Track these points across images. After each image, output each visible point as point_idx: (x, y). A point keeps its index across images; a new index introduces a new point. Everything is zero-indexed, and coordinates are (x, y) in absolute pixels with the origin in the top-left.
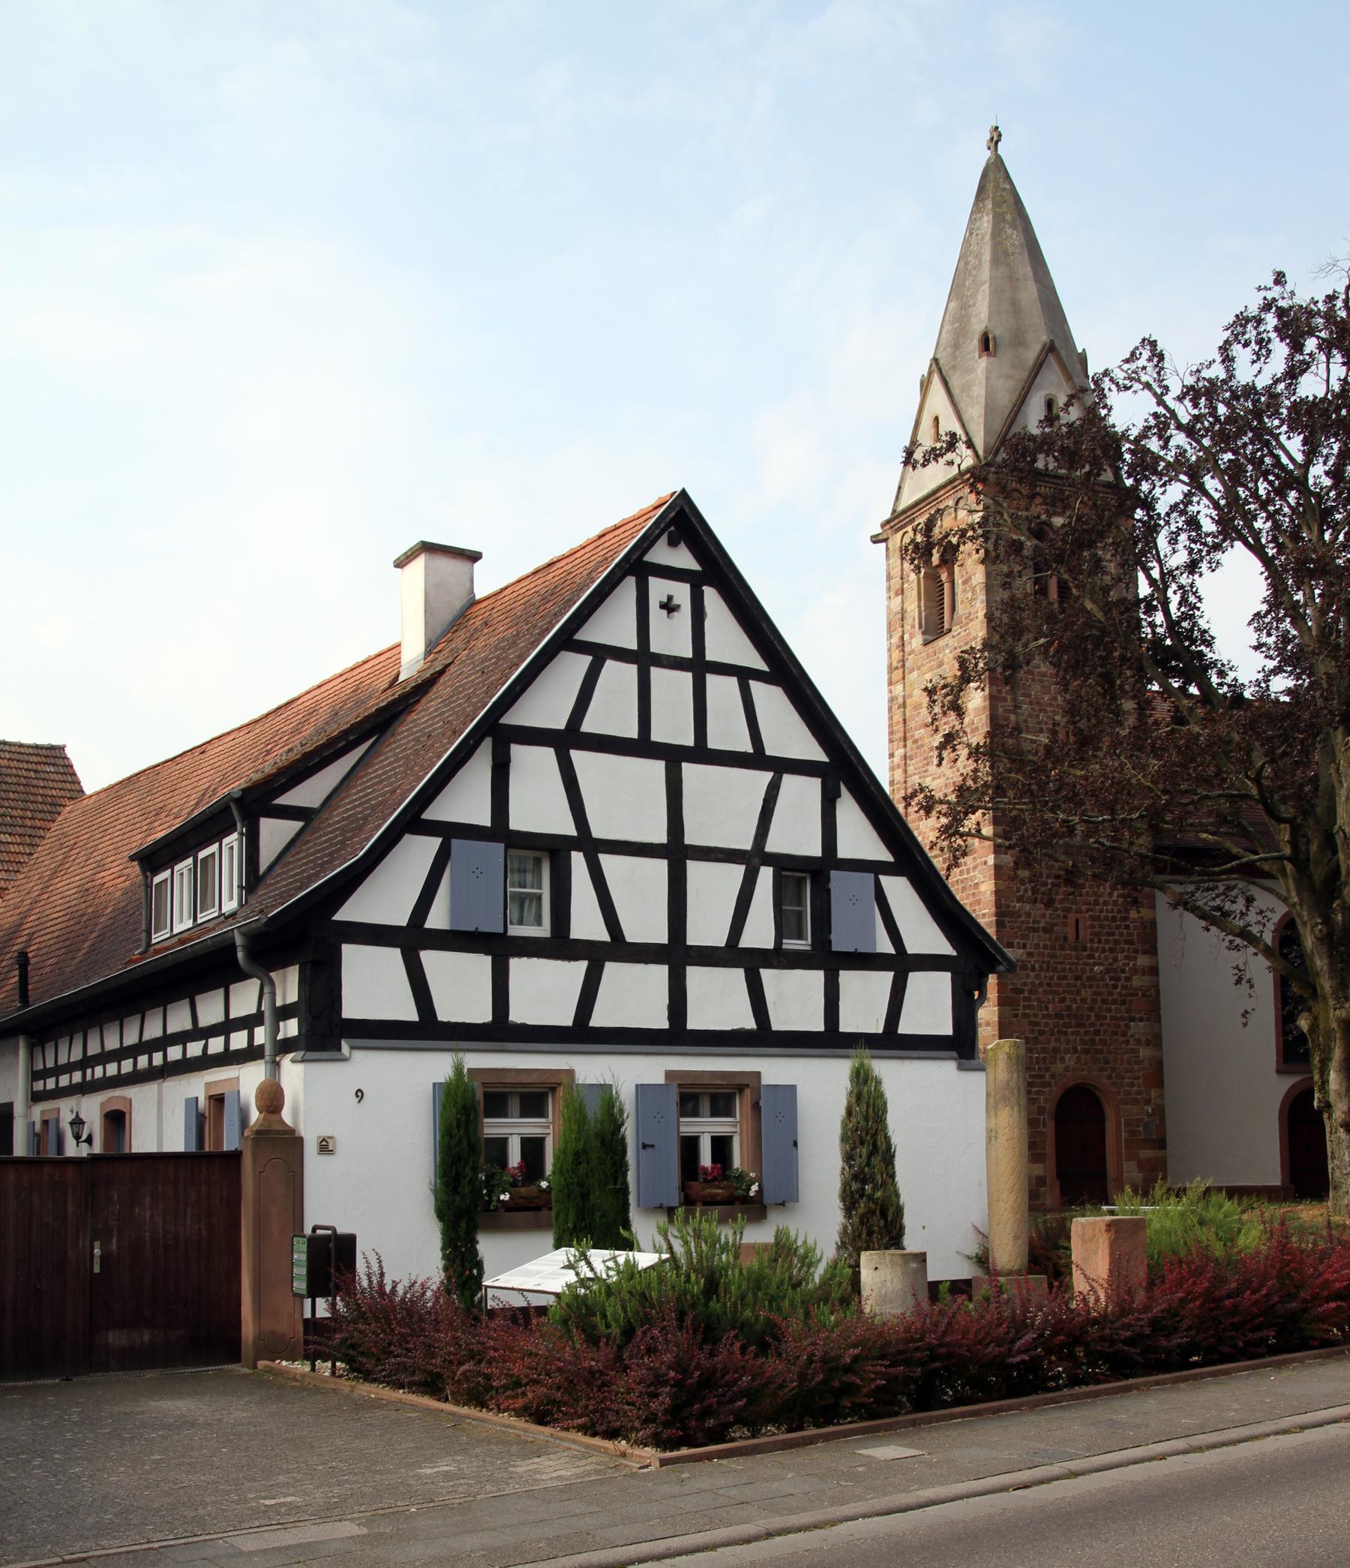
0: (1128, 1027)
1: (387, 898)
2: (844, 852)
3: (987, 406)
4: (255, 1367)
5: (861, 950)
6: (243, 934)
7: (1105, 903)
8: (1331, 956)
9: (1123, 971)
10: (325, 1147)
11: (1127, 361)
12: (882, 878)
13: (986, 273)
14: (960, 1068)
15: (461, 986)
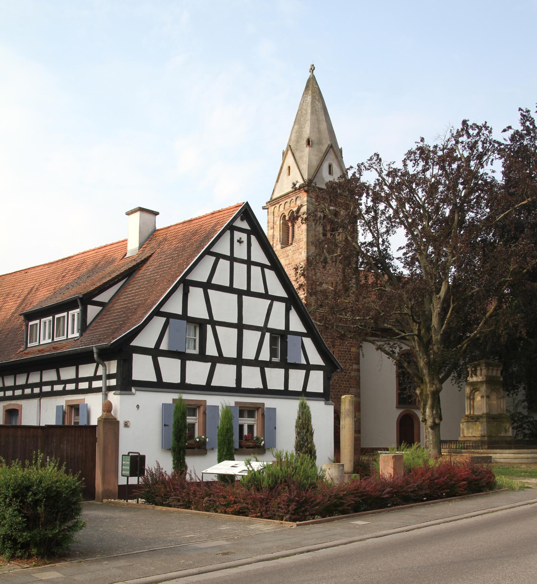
0: (349, 390)
1: (147, 339)
2: (291, 329)
3: (309, 165)
4: (102, 502)
5: (296, 362)
6: (97, 348)
8: (429, 369)
9: (348, 370)
10: (126, 425)
11: (369, 160)
13: (309, 117)
14: (326, 404)
15: (171, 369)
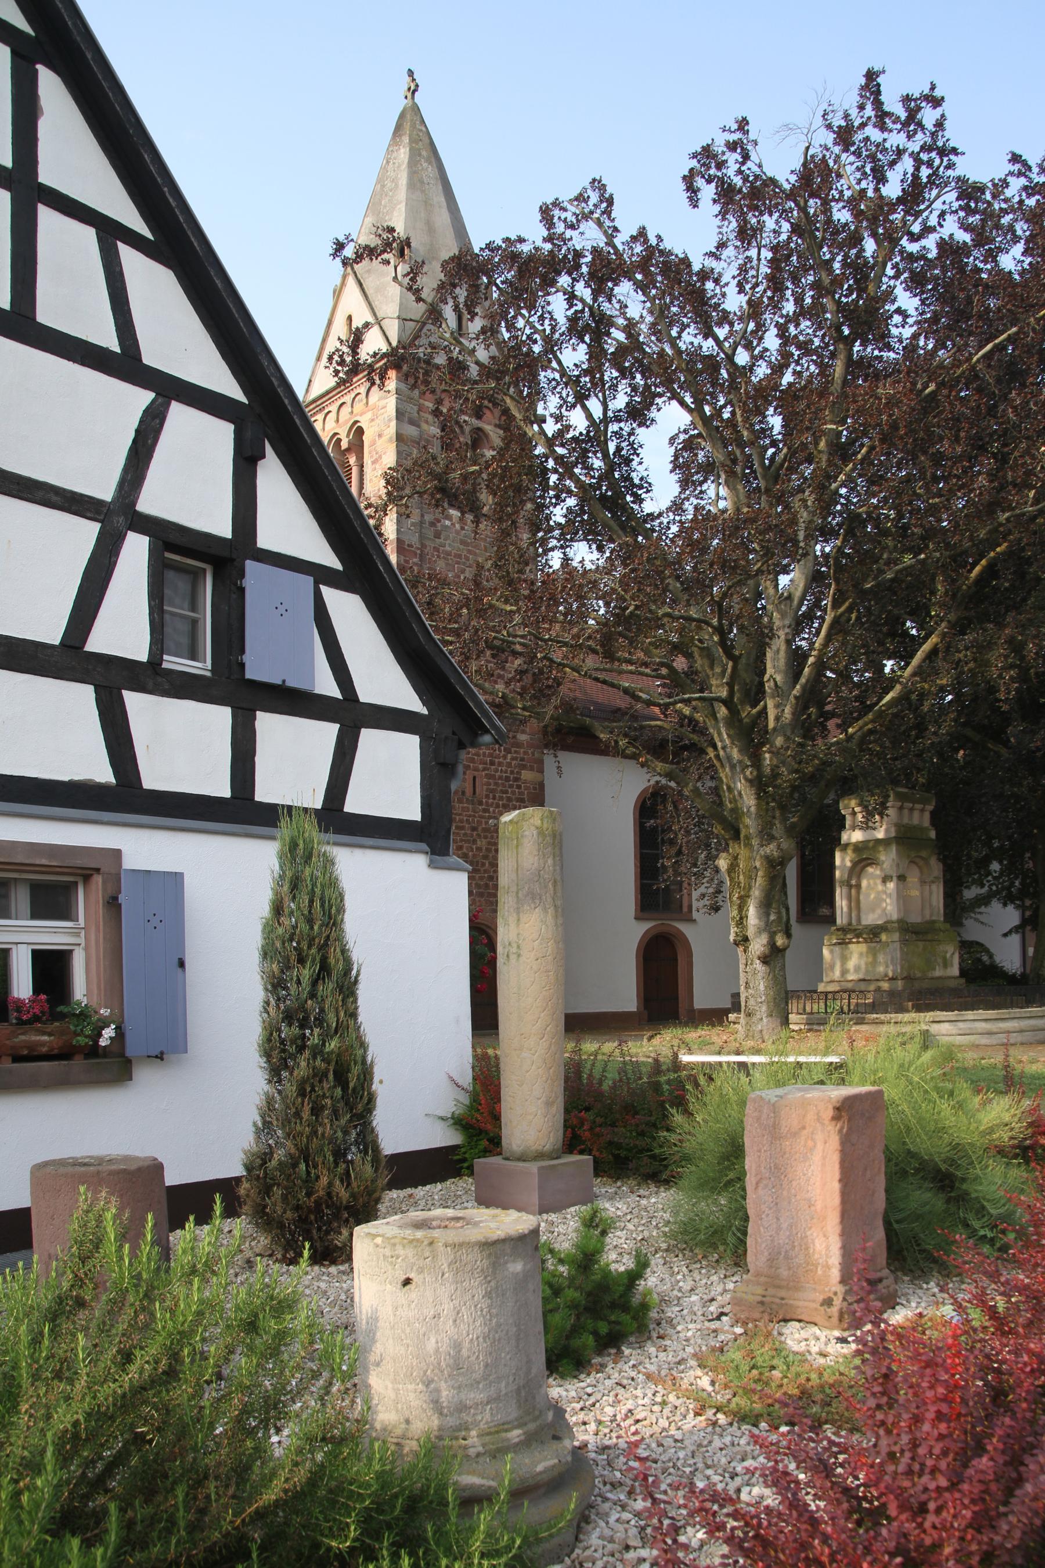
3: (401, 304)
5: (291, 683)
7: (500, 764)
8: (758, 798)
12: (323, 588)
13: (402, 194)
14: (432, 865)
